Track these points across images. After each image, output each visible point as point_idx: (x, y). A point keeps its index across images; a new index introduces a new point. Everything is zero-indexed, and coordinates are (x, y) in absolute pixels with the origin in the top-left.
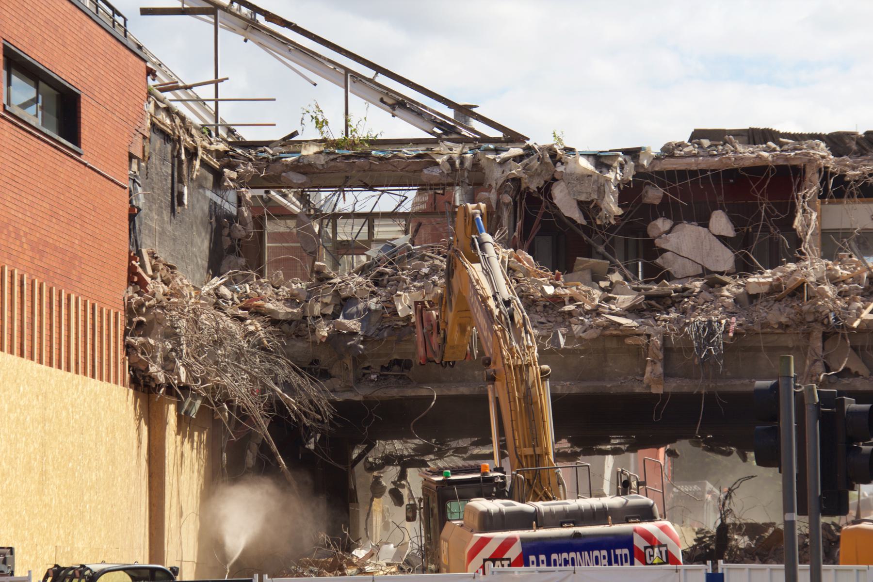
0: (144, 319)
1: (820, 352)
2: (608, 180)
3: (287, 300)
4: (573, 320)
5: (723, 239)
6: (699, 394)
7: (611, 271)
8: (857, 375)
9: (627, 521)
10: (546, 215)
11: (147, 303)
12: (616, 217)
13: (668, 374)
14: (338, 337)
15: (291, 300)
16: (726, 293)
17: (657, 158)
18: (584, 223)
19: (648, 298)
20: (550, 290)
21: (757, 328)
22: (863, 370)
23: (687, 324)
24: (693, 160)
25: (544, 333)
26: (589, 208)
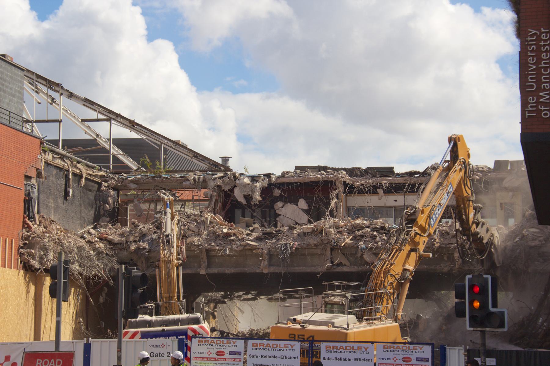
0: (27, 242)
1: (330, 256)
2: (256, 187)
3: (119, 235)
4: (234, 243)
5: (303, 210)
6: (281, 273)
7: (254, 223)
8: (345, 265)
9: (188, 324)
10: (232, 200)
11: (32, 236)
12: (259, 202)
13: (270, 265)
14: (138, 249)
15: (122, 235)
16: (295, 232)
17: (278, 178)
18: (246, 203)
19: (264, 234)
20: (225, 231)
21: (305, 246)
22: (347, 263)
23: (278, 245)
24: (292, 178)
25: (221, 248)
26: (248, 198)
